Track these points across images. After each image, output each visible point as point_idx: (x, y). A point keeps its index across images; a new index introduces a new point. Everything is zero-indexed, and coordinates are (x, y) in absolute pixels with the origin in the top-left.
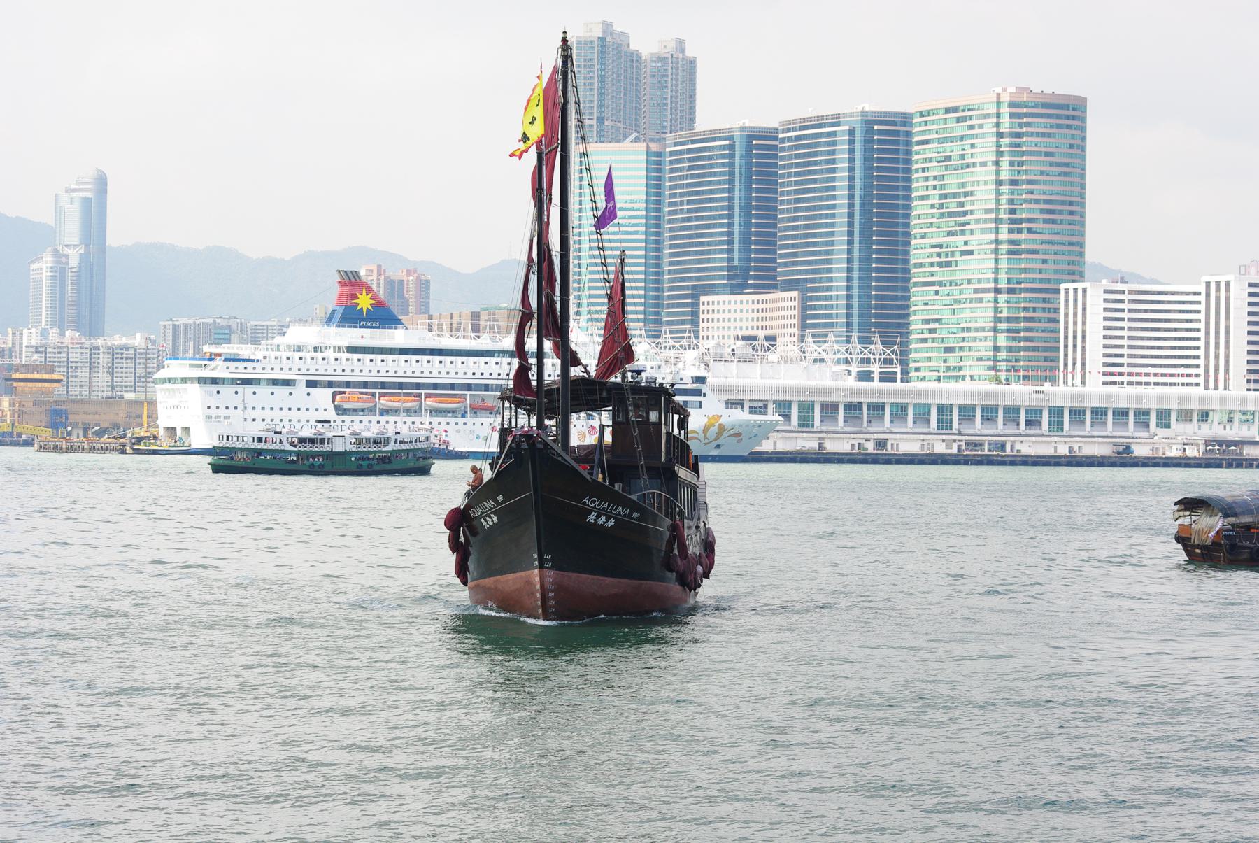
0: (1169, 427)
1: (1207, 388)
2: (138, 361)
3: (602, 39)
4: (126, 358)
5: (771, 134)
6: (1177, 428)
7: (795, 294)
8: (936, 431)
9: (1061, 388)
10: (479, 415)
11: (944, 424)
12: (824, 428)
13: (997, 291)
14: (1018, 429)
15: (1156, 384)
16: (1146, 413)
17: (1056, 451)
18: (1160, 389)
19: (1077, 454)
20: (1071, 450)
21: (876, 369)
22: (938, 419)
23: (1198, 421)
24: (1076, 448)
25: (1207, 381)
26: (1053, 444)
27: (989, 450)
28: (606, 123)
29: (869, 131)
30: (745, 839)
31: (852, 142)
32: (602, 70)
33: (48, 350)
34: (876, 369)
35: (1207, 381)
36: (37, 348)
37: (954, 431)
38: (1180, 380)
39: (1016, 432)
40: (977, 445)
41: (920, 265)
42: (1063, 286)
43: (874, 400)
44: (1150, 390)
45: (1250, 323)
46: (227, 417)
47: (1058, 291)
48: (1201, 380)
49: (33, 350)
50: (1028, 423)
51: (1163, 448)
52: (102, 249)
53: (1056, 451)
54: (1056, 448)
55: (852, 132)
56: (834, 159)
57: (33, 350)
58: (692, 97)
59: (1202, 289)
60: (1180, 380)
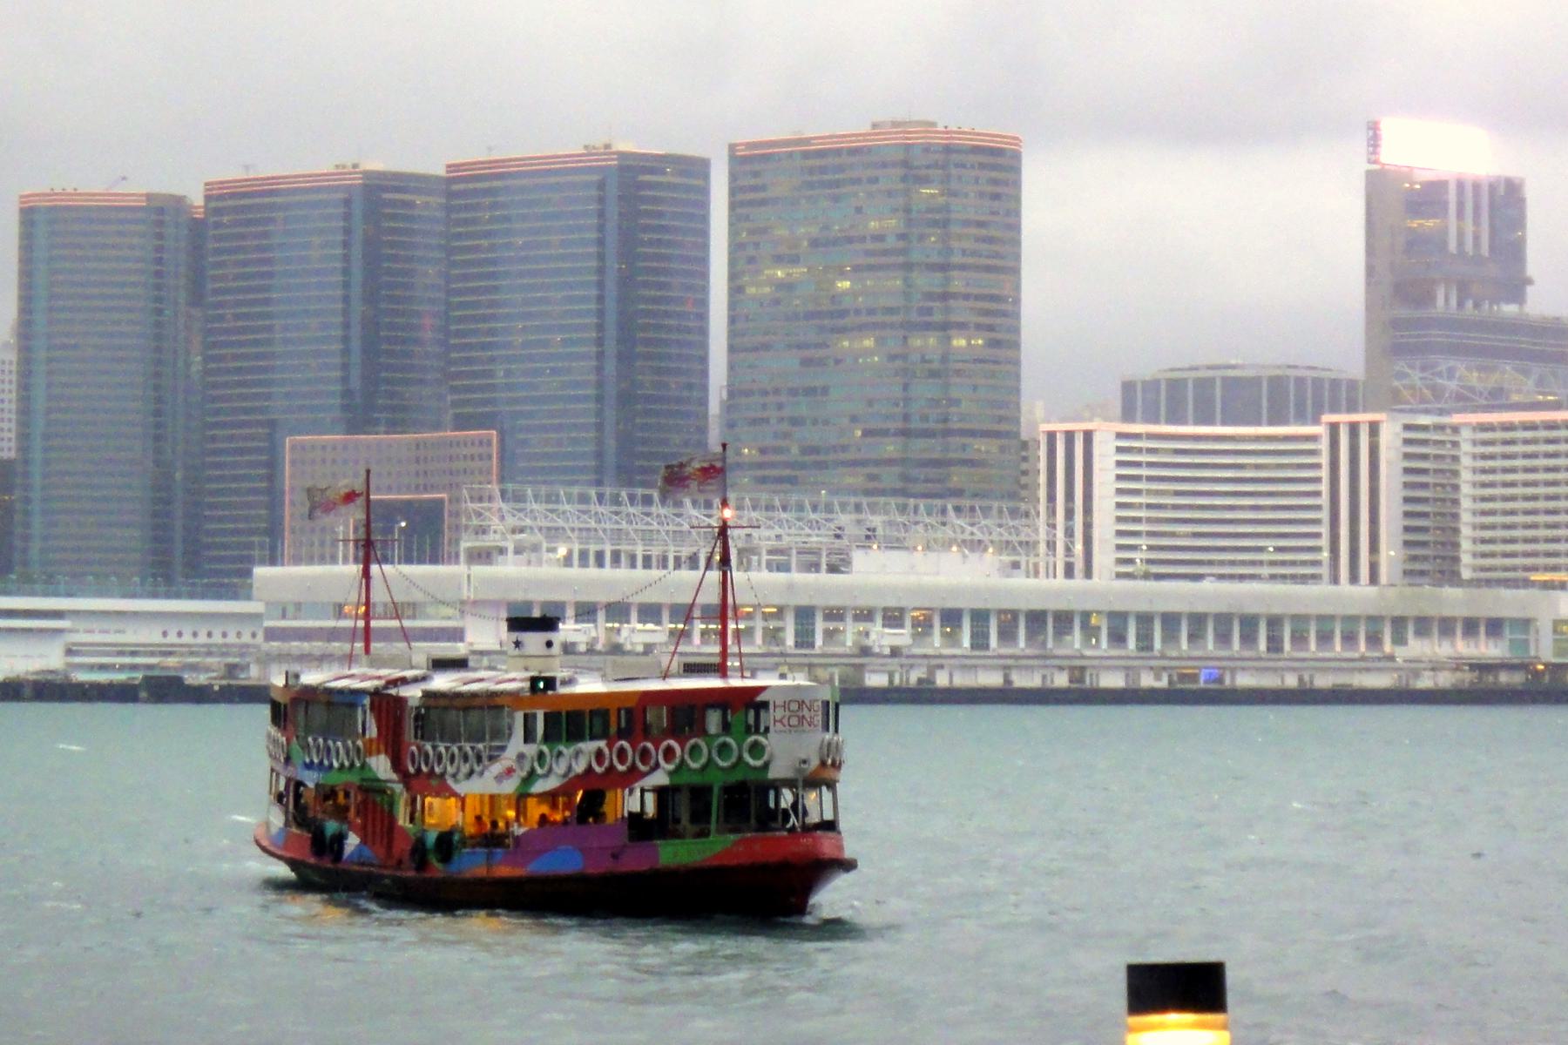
6: (1417, 647)
20: (1301, 679)
24: (1306, 678)
37: (1156, 653)
48: (1324, 571)
53: (1283, 681)
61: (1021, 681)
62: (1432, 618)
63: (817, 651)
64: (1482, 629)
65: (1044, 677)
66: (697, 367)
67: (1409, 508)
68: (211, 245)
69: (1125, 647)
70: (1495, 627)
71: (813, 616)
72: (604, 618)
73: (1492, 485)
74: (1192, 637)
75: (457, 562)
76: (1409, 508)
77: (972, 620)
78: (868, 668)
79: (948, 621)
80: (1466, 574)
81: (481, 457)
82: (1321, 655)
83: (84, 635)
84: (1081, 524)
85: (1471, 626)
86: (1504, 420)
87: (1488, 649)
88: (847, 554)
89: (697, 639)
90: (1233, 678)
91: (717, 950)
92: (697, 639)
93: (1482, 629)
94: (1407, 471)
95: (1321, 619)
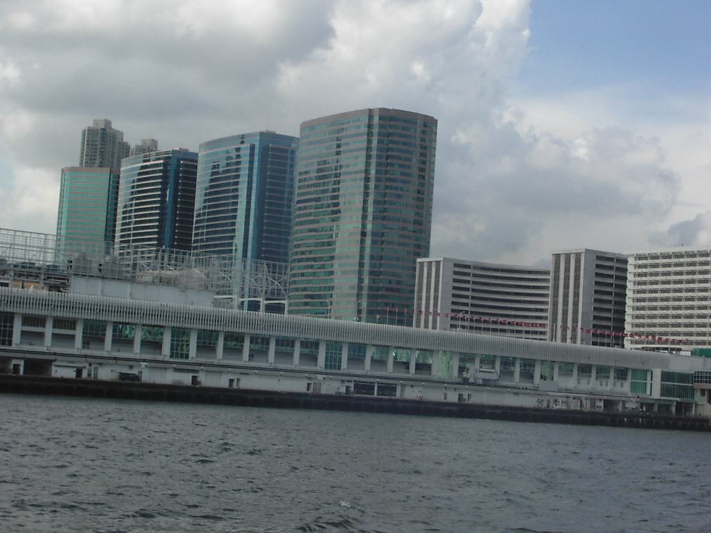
1: (553, 337)
8: (168, 359)
10: (91, 346)
11: (333, 362)
12: (419, 376)
15: (527, 332)
17: (445, 398)
19: (467, 402)
21: (263, 302)
22: (172, 345)
23: (615, 378)
24: (465, 397)
25: (554, 330)
27: (378, 394)
29: (264, 150)
31: (252, 155)
32: (102, 145)
34: (263, 302)
35: (554, 330)
39: (406, 376)
40: (368, 388)
45: (454, 295)
50: (145, 343)
51: (549, 401)
53: (445, 398)
54: (446, 394)
55: (252, 148)
61: (207, 380)
62: (575, 363)
63: (14, 347)
65: (231, 381)
68: (297, 198)
72: (51, 326)
73: (643, 308)
75: (411, 326)
78: (54, 363)
79: (582, 371)
83: (490, 378)
86: (366, 249)
87: (610, 387)
88: (68, 280)
89: (48, 339)
90: (402, 391)
92: (48, 339)
94: (596, 300)
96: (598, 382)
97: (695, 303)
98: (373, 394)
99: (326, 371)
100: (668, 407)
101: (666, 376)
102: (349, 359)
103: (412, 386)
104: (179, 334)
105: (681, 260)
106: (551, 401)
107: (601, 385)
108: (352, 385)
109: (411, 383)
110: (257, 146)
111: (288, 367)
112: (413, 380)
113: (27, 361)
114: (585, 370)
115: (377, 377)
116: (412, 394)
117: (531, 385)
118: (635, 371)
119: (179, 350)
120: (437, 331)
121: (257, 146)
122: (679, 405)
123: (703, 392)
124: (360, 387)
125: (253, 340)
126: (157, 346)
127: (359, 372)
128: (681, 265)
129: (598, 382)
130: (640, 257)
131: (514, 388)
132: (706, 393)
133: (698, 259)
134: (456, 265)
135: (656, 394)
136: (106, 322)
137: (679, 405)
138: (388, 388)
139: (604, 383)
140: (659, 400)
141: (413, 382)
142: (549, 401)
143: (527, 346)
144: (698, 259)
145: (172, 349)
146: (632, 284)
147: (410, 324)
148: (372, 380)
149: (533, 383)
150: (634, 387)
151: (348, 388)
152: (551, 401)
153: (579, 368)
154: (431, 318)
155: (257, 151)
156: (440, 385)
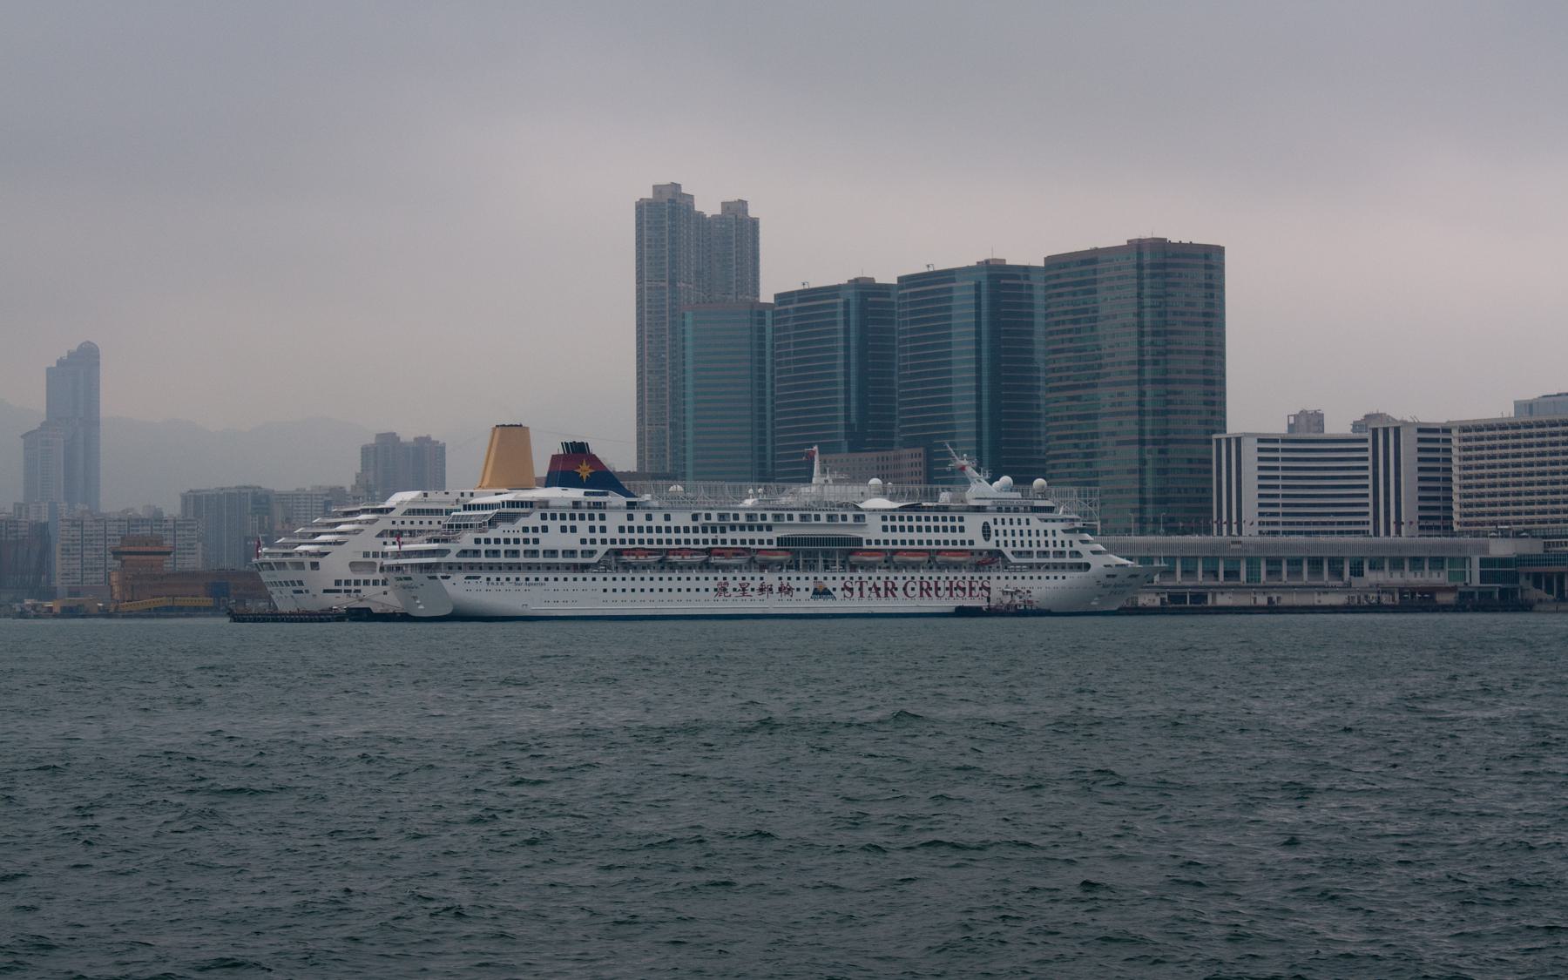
0: (1363, 575)
2: (178, 533)
3: (672, 201)
4: (166, 530)
5: (885, 289)
6: (1371, 577)
7: (921, 450)
8: (1245, 584)
9: (1214, 538)
13: (1142, 443)
14: (1217, 580)
16: (1341, 561)
17: (1255, 602)
18: (1293, 538)
20: (1270, 600)
24: (1275, 599)
26: (1253, 595)
28: (678, 285)
30: (744, 975)
33: (85, 523)
36: (73, 521)
37: (1155, 584)
38: (1336, 528)
39: (1216, 583)
40: (1182, 598)
41: (1128, 413)
42: (1215, 436)
43: (1335, 555)
44: (1323, 539)
46: (357, 591)
47: (1209, 442)
48: (1370, 528)
49: (69, 524)
50: (1227, 574)
51: (1359, 598)
52: (91, 420)
53: (1255, 602)
54: (1255, 599)
55: (847, 304)
56: (950, 316)
57: (69, 524)
58: (756, 257)
59: (1369, 435)
60: (1336, 528)
62: (1424, 558)
64: (1387, 565)
66: (1217, 378)
67: (1423, 474)
69: (1239, 580)
70: (1437, 563)
71: (1280, 564)
74: (1185, 572)
76: (1423, 474)
77: (1247, 564)
80: (1456, 528)
81: (1444, 460)
82: (1292, 583)
84: (549, 489)
85: (1417, 562)
90: (1214, 598)
91: (1437, 737)
93: (1387, 565)
95: (1184, 559)
96: (1413, 574)
97: (1522, 479)
98: (1186, 603)
99: (1249, 584)
100: (1491, 594)
101: (1483, 562)
102: (1203, 572)
103: (1222, 593)
104: (1252, 562)
105: (1506, 432)
106: (1362, 597)
107: (1416, 576)
108: (1166, 596)
109: (1220, 590)
110: (853, 301)
111: (1300, 583)
112: (1223, 587)
113: (1169, 596)
114: (1417, 562)
115: (1188, 587)
116: (1223, 600)
117: (1341, 582)
118: (1452, 559)
119: (1253, 574)
120: (1404, 539)
121: (853, 301)
122: (1502, 591)
123: (1528, 575)
124: (1172, 598)
125: (1289, 563)
126: (1236, 574)
127: (1170, 584)
128: (1506, 437)
129: (1413, 574)
130: (1465, 429)
131: (1324, 587)
132: (1531, 577)
133: (1522, 431)
134: (1260, 441)
135: (1476, 582)
136: (1322, 558)
137: (1502, 591)
138: (1199, 597)
139: (1419, 574)
140: (1479, 587)
141: (1222, 589)
142: (1359, 598)
143: (1332, 546)
144: (1522, 431)
145: (1247, 575)
146: (1457, 468)
147: (1208, 531)
148: (1183, 590)
149: (1343, 580)
150: (1451, 575)
151: (1162, 600)
152: (1362, 597)
153: (1370, 562)
154: (1225, 519)
155: (853, 308)
156: (1312, 590)
